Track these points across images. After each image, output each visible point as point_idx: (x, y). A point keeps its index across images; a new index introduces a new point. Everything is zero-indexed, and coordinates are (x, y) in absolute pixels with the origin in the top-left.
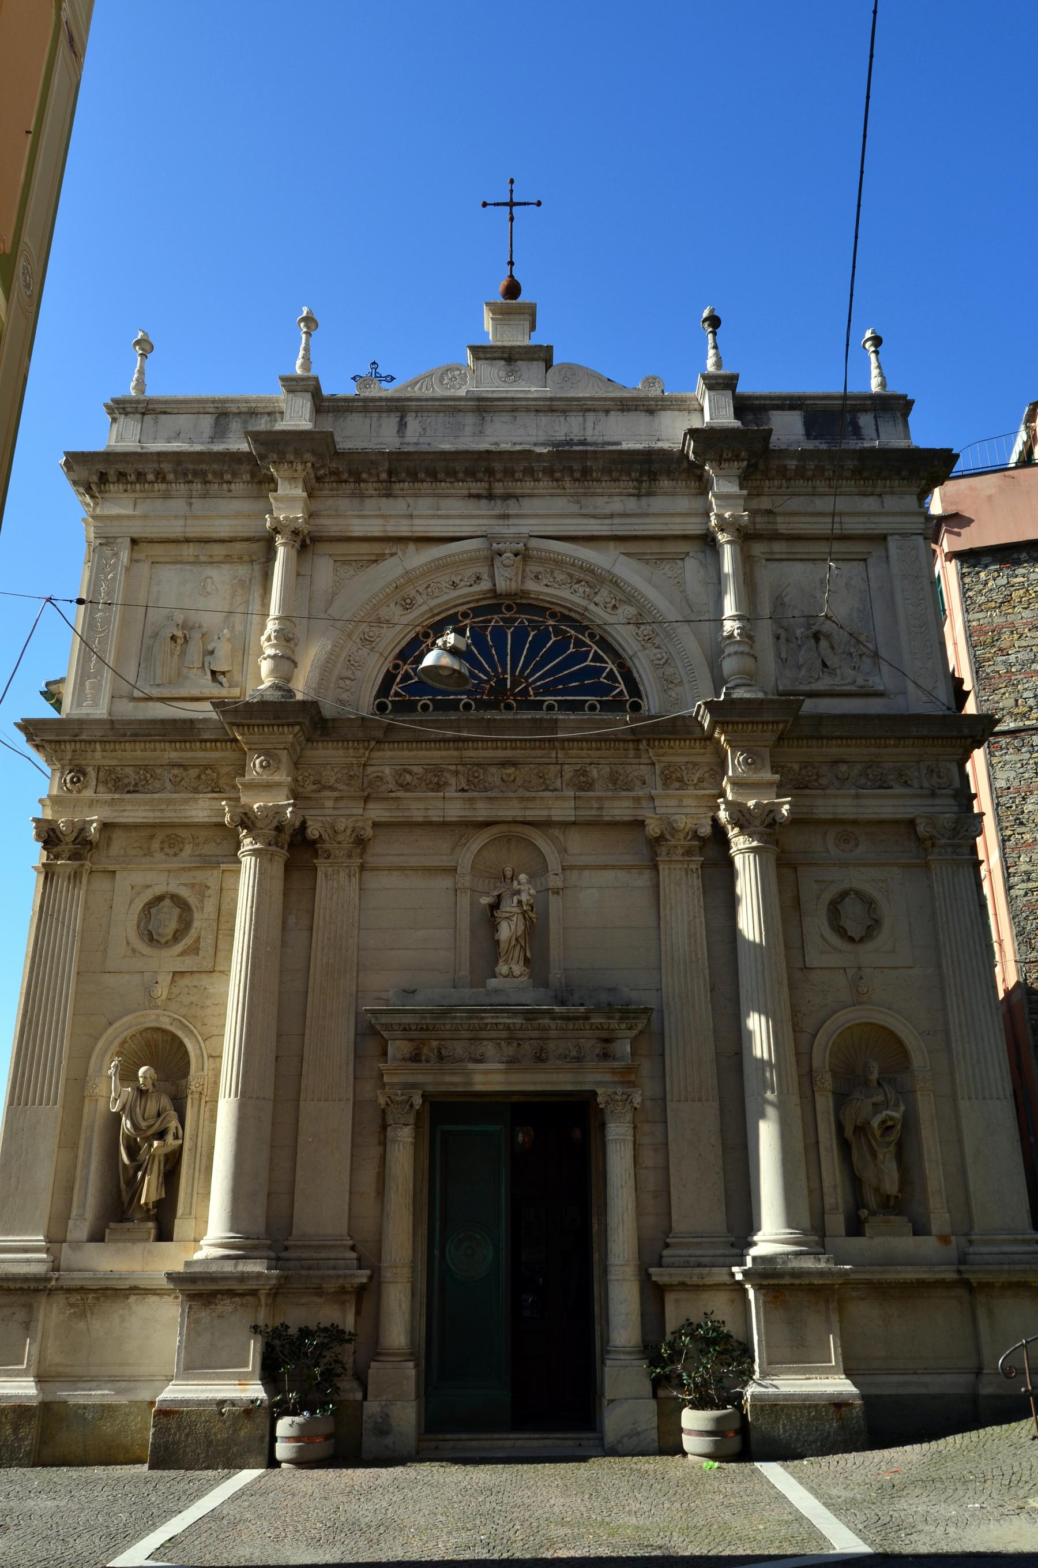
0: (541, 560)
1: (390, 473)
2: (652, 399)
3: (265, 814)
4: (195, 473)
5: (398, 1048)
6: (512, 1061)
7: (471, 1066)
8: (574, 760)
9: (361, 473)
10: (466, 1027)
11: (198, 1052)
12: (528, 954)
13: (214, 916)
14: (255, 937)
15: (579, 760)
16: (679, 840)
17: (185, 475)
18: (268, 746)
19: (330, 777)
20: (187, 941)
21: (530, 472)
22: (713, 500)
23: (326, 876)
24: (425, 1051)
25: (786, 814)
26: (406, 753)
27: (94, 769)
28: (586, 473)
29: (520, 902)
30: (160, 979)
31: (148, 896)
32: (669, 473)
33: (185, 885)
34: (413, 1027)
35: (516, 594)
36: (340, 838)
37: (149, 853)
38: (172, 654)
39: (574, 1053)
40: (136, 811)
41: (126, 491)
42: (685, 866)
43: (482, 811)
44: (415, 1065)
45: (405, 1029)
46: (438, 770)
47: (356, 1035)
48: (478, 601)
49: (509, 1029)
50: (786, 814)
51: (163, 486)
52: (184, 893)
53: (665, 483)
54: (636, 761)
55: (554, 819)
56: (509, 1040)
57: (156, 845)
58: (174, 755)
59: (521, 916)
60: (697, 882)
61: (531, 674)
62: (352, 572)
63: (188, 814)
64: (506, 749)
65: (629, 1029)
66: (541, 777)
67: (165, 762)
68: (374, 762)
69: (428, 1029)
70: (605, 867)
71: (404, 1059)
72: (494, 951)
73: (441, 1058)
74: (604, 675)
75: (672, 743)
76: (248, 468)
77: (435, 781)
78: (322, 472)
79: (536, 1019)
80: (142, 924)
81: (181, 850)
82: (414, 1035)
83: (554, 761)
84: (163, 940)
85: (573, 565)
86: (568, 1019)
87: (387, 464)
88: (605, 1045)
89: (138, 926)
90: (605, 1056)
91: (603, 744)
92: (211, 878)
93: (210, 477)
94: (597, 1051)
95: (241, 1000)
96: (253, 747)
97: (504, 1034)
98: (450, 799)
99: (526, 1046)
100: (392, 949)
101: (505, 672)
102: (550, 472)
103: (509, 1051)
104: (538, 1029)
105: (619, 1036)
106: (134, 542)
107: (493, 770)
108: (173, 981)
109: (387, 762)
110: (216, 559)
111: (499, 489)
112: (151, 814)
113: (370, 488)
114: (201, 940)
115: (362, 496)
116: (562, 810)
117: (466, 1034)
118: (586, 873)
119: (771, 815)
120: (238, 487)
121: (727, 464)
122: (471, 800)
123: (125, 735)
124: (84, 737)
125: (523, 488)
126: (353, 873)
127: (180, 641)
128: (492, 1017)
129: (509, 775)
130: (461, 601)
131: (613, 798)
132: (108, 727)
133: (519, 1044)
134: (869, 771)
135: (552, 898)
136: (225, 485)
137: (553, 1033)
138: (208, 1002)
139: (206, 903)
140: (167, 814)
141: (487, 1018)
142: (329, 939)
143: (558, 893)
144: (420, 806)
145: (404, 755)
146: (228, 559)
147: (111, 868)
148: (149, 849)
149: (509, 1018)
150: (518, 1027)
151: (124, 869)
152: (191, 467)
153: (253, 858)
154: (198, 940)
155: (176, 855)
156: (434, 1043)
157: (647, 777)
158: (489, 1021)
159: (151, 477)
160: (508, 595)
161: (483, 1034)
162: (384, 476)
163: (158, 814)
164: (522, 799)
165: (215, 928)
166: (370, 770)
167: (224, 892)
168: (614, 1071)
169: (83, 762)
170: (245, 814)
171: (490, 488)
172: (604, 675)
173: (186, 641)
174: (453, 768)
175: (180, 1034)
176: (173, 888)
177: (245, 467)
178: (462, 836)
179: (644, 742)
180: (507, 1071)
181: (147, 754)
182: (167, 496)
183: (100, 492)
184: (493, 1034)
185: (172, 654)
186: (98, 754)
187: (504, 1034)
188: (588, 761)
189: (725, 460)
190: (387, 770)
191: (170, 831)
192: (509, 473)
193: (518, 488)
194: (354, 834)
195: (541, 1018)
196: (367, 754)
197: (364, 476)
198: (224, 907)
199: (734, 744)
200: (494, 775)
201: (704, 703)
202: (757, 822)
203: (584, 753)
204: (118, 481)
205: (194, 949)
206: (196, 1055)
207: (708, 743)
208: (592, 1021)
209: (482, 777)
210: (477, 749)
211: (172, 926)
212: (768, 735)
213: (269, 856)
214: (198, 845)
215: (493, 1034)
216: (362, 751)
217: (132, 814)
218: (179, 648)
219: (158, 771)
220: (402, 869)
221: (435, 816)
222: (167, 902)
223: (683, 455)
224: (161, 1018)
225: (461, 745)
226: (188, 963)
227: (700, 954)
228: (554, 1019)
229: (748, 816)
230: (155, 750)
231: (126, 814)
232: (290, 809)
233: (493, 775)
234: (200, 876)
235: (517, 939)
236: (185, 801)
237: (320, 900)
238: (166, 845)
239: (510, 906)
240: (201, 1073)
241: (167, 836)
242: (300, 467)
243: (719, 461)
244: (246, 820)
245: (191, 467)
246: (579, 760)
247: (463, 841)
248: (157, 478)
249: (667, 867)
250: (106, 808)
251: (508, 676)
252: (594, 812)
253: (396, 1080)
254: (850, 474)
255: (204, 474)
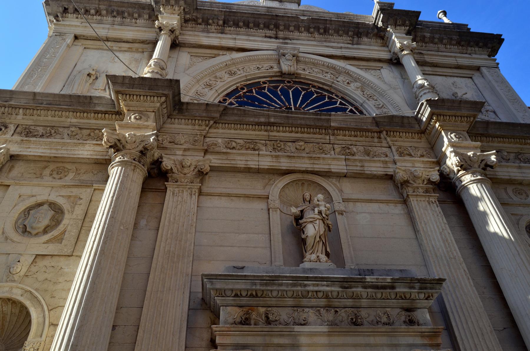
0: (305, 63)
1: (224, 23)
2: (352, 15)
3: (134, 139)
4: (118, 13)
5: (228, 313)
6: (332, 324)
7: (297, 328)
8: (341, 142)
9: (209, 19)
10: (290, 294)
11: (41, 320)
12: (328, 250)
13: (81, 217)
14: (112, 217)
15: (344, 142)
16: (419, 184)
17: (113, 11)
18: (142, 109)
19: (181, 139)
20: (55, 233)
21: (298, 28)
22: (396, 40)
23: (173, 194)
24: (254, 316)
25: (495, 160)
26: (233, 131)
27: (14, 126)
28: (326, 31)
29: (320, 213)
30: (22, 259)
31: (31, 202)
32: (367, 35)
33: (63, 196)
34: (244, 294)
35: (293, 74)
36: (186, 171)
37: (41, 176)
38: (86, 82)
39: (384, 319)
40: (37, 148)
41: (77, 18)
42: (427, 199)
43: (285, 164)
44: (245, 328)
45: (236, 295)
46: (253, 142)
47: (189, 309)
48: (271, 77)
49: (327, 297)
50: (495, 160)
51: (99, 18)
52: (61, 201)
53: (365, 39)
54: (379, 144)
55: (333, 170)
56: (328, 307)
57: (47, 172)
58: (74, 120)
59: (321, 222)
60: (438, 209)
61: (306, 107)
62: (201, 60)
63: (76, 152)
64: (297, 132)
65: (426, 299)
66: (321, 149)
67: (67, 124)
68: (210, 135)
69: (257, 296)
70: (371, 201)
71: (235, 323)
72: (301, 243)
73: (268, 321)
74: (348, 111)
75: (401, 134)
76: (148, 12)
77: (252, 146)
78: (188, 16)
79: (350, 287)
80: (20, 221)
81: (66, 176)
82: (244, 301)
83: (328, 141)
84: (34, 232)
85: (323, 65)
86: (377, 287)
87: (223, 17)
88: (409, 313)
89: (16, 222)
90: (411, 322)
91: (358, 133)
92: (85, 193)
93: (126, 14)
94: (403, 318)
95: (90, 263)
96: (131, 109)
97: (323, 302)
98: (263, 155)
99: (342, 313)
100: (221, 246)
101: (290, 104)
102: (308, 30)
103: (330, 316)
104: (352, 298)
105: (419, 305)
106: (76, 38)
107: (290, 144)
108: (34, 261)
109: (220, 135)
110: (123, 49)
111: (281, 34)
112: (49, 151)
113: (213, 28)
114: (67, 233)
115: (208, 32)
116: (338, 166)
117: (290, 302)
118: (358, 204)
119: (484, 163)
120: (140, 21)
121: (399, 27)
122: (277, 157)
123: (42, 104)
124: (12, 103)
125: (293, 35)
126: (193, 192)
127: (93, 77)
128: (314, 285)
129: (301, 146)
130: (262, 75)
131: (370, 161)
132: (31, 97)
133: (336, 312)
134: (520, 157)
135: (339, 217)
136: (133, 20)
137: (364, 302)
138: (61, 279)
139: (76, 208)
140: (59, 152)
141: (309, 285)
142: (172, 234)
143: (342, 214)
144: (240, 160)
145: (232, 132)
146: (130, 50)
147: (7, 182)
148: (41, 174)
149: (327, 286)
150: (335, 294)
151: (17, 184)
152: (116, 8)
153: (120, 168)
154: (64, 232)
155: (61, 179)
156: (262, 310)
157: (388, 153)
158: (311, 288)
159: (93, 12)
160: (289, 74)
161: (304, 302)
162: (221, 22)
163: (54, 151)
164: (310, 158)
165: (80, 225)
166: (208, 140)
167: (92, 203)
168: (422, 335)
169: (8, 121)
170: (119, 140)
171: (276, 34)
172: (348, 111)
173: (97, 78)
174: (264, 142)
175: (28, 303)
176: (53, 198)
177: (146, 11)
178: (270, 180)
179: (384, 132)
180: (329, 334)
181: (56, 119)
182: (100, 22)
183: (62, 17)
184: (314, 302)
185: (86, 82)
186: (20, 117)
187: (323, 302)
188: (350, 143)
189: (398, 25)
190: (220, 140)
191: (60, 165)
192: (287, 28)
193: (290, 35)
194: (196, 170)
195: (355, 287)
196: (207, 129)
197: (210, 21)
198: (90, 212)
199: (445, 128)
200: (291, 147)
201: (427, 101)
202: (476, 165)
203: (347, 138)
204: (74, 13)
205: (59, 239)
206: (38, 323)
207: (422, 135)
208: (397, 290)
209: (282, 147)
210: (279, 132)
211: (46, 222)
212: (464, 124)
213: (133, 167)
214: (79, 174)
215: (314, 302)
216: (204, 127)
217: (34, 150)
218: (91, 80)
219: (61, 130)
220: (229, 195)
221: (253, 164)
222: (46, 207)
223: (375, 26)
224: (15, 291)
225: (269, 128)
226: (52, 249)
227: (454, 252)
228: (365, 287)
229: (469, 162)
230: (61, 117)
231: (29, 150)
232: (153, 138)
233: (289, 147)
234: (75, 191)
235: (320, 237)
236: (76, 145)
237: (168, 208)
238: (55, 173)
239: (309, 215)
240: (39, 339)
241: (56, 165)
242: (177, 8)
243: (395, 25)
244: (118, 144)
245: (116, 8)
246: (344, 142)
247: (271, 182)
248: (96, 14)
249: (415, 199)
250: (16, 145)
251: (293, 107)
252: (358, 168)
253: (228, 340)
254: (455, 42)
255: (123, 12)
